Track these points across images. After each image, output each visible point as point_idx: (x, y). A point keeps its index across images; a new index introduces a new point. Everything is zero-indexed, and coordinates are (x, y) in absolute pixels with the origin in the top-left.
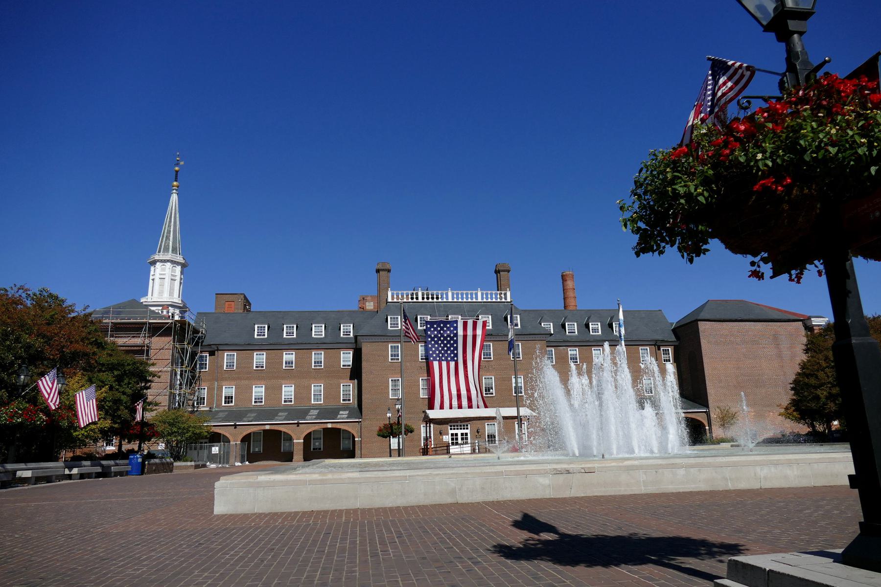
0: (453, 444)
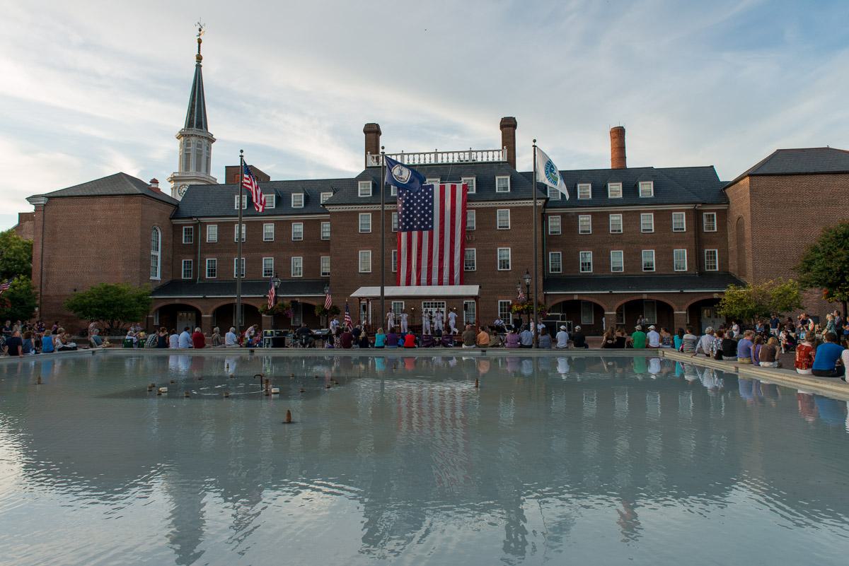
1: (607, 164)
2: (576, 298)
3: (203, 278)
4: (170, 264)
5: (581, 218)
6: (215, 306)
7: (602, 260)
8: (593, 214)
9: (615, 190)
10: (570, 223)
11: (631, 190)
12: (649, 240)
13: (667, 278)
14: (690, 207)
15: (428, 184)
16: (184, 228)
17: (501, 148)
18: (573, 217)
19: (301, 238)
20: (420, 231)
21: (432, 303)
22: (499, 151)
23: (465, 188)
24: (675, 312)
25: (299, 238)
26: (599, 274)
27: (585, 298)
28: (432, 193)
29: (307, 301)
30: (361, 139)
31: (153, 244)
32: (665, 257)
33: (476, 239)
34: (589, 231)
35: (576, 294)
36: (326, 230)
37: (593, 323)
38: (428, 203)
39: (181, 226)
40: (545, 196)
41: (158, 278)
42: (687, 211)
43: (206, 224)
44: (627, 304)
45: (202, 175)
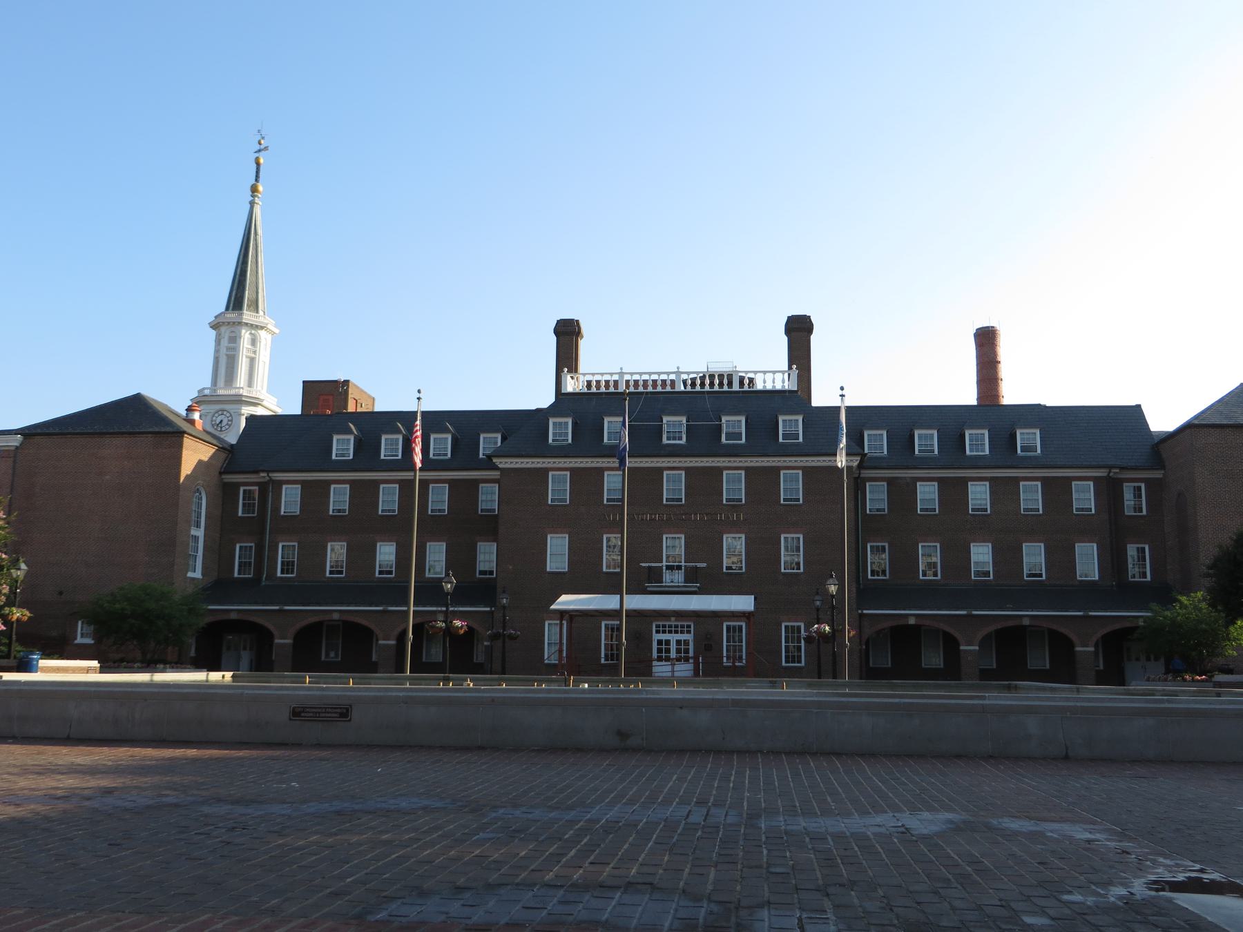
0: (660, 659)
1: (969, 397)
2: (912, 621)
4: (218, 552)
6: (299, 626)
7: (957, 558)
8: (941, 481)
9: (978, 441)
10: (902, 493)
11: (1004, 441)
12: (1033, 528)
13: (1061, 587)
16: (242, 489)
17: (786, 368)
19: (344, 511)
21: (670, 626)
22: (783, 372)
24: (277, 641)
25: (440, 510)
27: (927, 622)
30: (550, 343)
31: (194, 517)
32: (1061, 558)
33: (745, 520)
35: (912, 614)
36: (489, 498)
37: (1048, 667)
39: (238, 485)
40: (860, 451)
41: (198, 574)
42: (1096, 480)
43: (280, 484)
44: (998, 632)
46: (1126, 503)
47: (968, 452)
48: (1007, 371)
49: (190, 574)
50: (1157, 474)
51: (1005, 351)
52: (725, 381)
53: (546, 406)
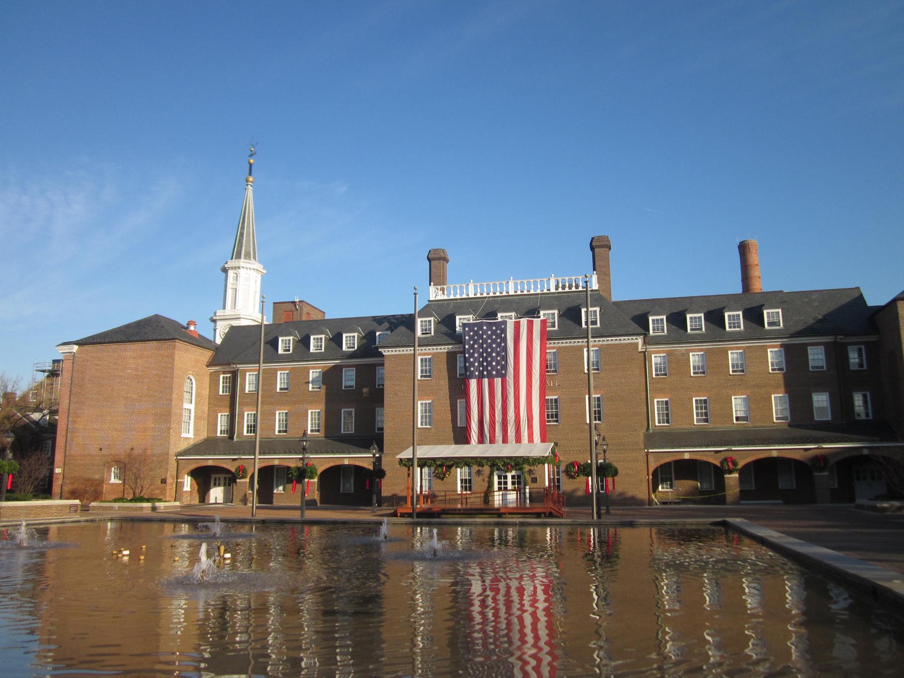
3: (241, 434)
5: (810, 350)
14: (828, 339)
15: (500, 320)
18: (683, 354)
20: (491, 378)
23: (544, 322)
26: (718, 425)
28: (504, 331)
29: (357, 463)
34: (823, 367)
37: (795, 487)
38: (500, 343)
41: (191, 435)
42: (826, 345)
45: (229, 313)
46: (852, 361)
47: (727, 329)
48: (756, 272)
49: (184, 435)
50: (873, 338)
51: (754, 258)
52: (560, 285)
53: (883, 304)
